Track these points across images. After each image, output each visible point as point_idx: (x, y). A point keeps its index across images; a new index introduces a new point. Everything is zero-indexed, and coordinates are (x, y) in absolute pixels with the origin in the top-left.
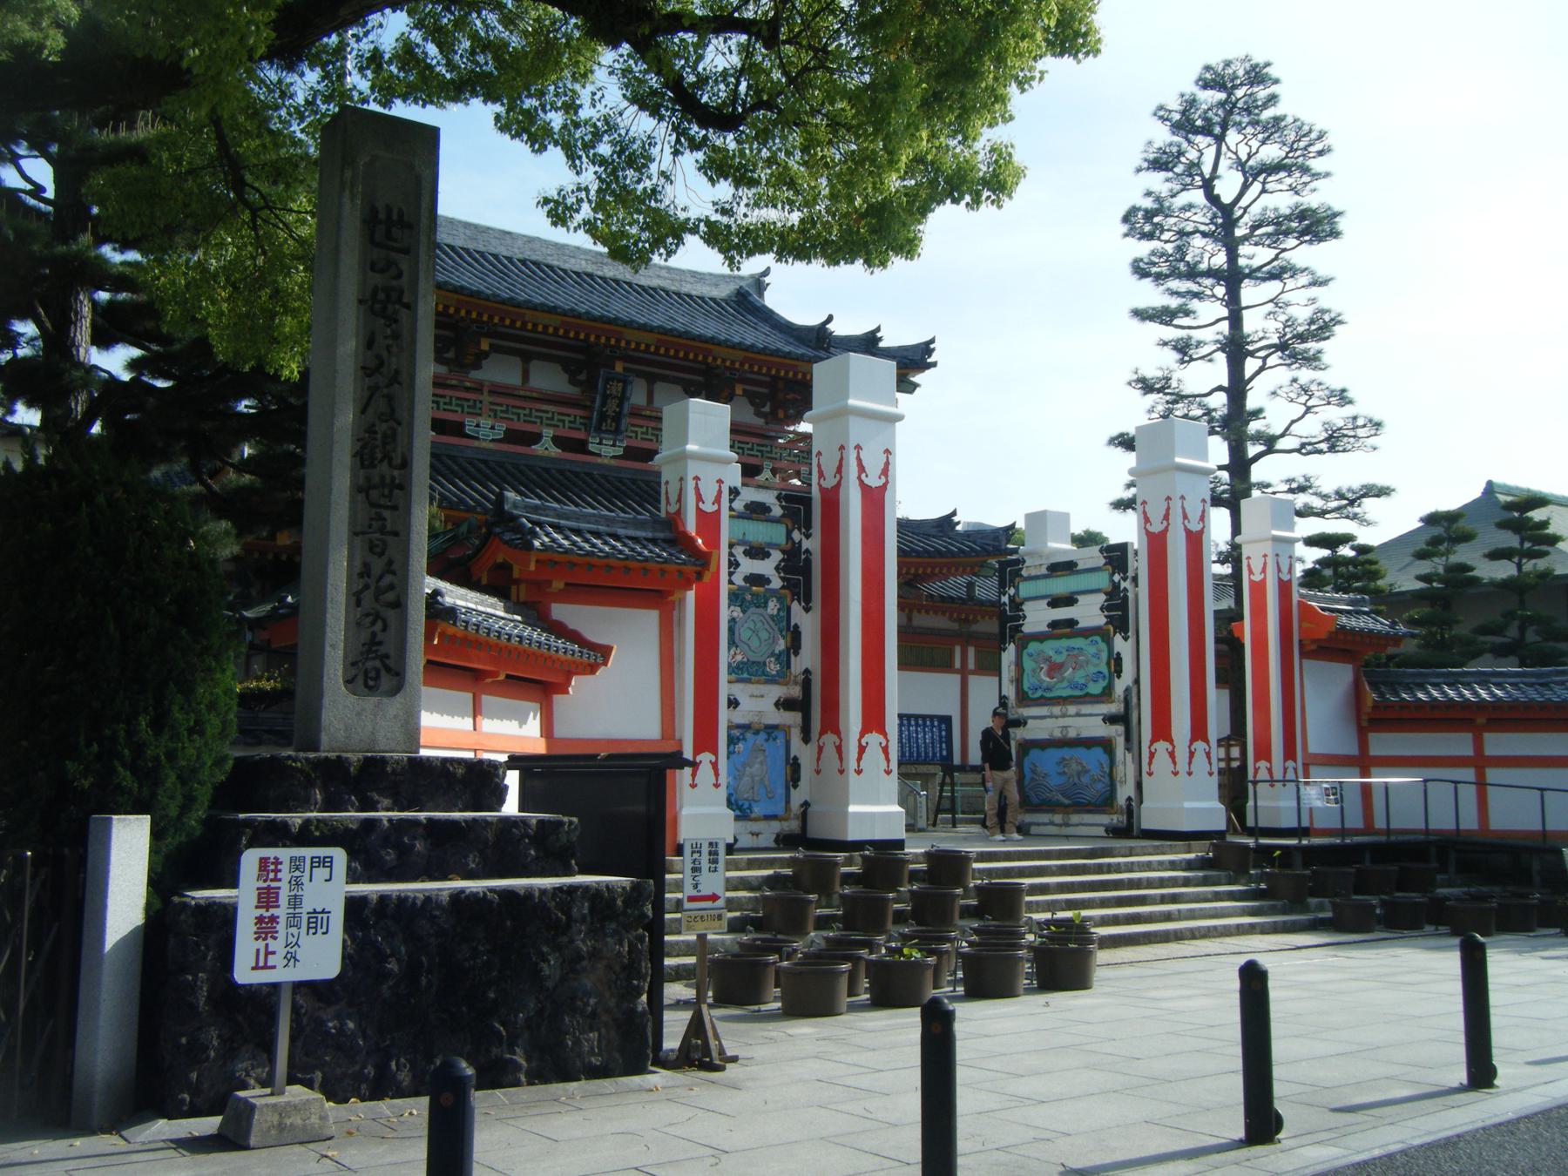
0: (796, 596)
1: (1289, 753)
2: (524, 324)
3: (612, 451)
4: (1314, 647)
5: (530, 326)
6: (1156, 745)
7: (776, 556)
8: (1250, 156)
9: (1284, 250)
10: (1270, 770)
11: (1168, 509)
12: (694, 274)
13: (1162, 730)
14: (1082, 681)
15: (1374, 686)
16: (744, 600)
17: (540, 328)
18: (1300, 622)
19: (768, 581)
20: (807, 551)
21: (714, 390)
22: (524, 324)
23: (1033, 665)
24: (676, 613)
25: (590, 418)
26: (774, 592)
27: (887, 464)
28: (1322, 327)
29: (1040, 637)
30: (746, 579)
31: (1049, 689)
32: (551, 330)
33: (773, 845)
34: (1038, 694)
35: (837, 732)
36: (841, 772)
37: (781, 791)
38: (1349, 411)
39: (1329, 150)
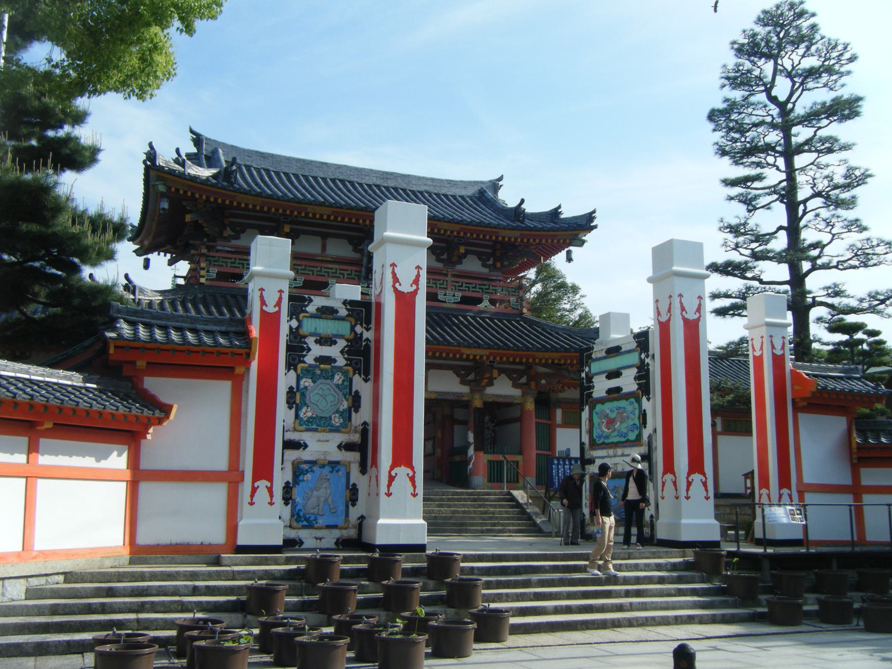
0: (357, 370)
1: (784, 481)
2: (307, 214)
4: (805, 404)
5: (311, 215)
7: (342, 343)
8: (793, 68)
9: (820, 128)
11: (670, 304)
12: (449, 182)
14: (625, 431)
15: (862, 432)
17: (318, 216)
18: (793, 385)
19: (335, 361)
20: (367, 339)
21: (272, 227)
22: (307, 214)
24: (244, 382)
25: (361, 272)
26: (339, 369)
27: (700, 305)
28: (855, 179)
29: (602, 401)
30: (316, 360)
31: (607, 437)
32: (325, 217)
33: (334, 546)
34: (602, 440)
35: (673, 473)
37: (342, 508)
38: (865, 235)
39: (856, 58)
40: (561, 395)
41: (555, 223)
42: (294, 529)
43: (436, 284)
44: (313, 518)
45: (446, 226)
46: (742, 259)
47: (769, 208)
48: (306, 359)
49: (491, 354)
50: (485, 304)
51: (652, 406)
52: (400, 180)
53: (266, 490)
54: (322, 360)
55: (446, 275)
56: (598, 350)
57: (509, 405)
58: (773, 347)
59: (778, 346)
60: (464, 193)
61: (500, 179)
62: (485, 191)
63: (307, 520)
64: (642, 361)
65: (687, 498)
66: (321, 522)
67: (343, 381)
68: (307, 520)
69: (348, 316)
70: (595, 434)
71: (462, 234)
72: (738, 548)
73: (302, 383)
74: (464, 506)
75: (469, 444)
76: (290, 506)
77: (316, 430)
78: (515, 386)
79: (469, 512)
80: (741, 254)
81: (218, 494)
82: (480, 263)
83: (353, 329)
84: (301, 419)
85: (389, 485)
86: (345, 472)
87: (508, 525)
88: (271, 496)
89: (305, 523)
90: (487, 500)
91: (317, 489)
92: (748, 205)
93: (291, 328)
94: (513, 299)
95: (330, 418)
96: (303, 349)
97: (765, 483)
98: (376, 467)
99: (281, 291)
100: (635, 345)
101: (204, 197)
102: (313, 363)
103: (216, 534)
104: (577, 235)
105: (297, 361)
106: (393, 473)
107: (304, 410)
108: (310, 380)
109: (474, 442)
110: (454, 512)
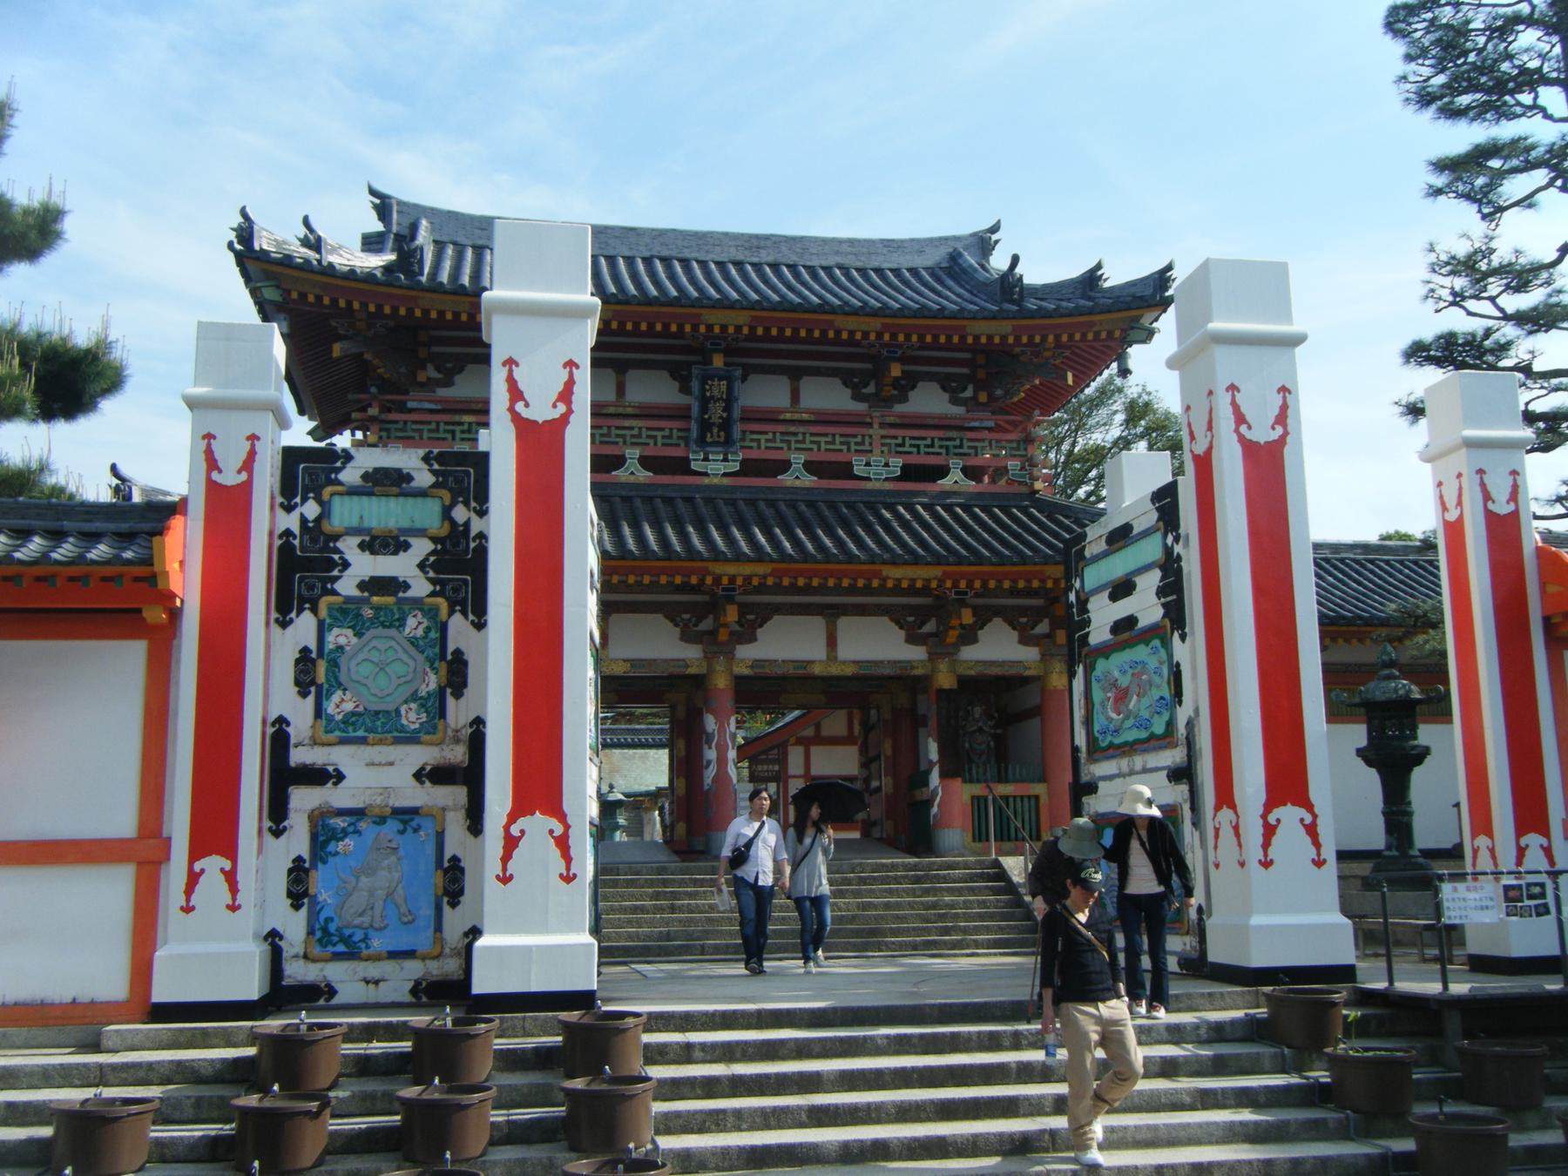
3: (722, 468)
7: (421, 548)
10: (1548, 851)
16: (359, 615)
25: (688, 430)
26: (417, 603)
27: (1284, 408)
29: (1105, 650)
30: (362, 586)
33: (408, 998)
35: (1233, 806)
37: (427, 912)
41: (1090, 299)
42: (314, 961)
43: (848, 444)
44: (358, 936)
45: (850, 323)
46: (1477, 325)
47: (1530, 206)
48: (338, 586)
49: (947, 575)
50: (954, 479)
51: (1189, 652)
53: (222, 877)
54: (376, 585)
55: (870, 425)
56: (1096, 535)
57: (1025, 681)
58: (1487, 497)
60: (920, 262)
61: (995, 229)
62: (960, 255)
63: (346, 940)
64: (1168, 551)
65: (1267, 864)
66: (378, 944)
67: (428, 630)
69: (435, 485)
70: (1096, 727)
71: (887, 337)
72: (1391, 981)
74: (891, 892)
75: (931, 764)
76: (304, 910)
77: (363, 741)
78: (1025, 640)
79: (898, 906)
80: (1470, 313)
81: (112, 889)
82: (848, 392)
83: (446, 513)
84: (330, 719)
85: (506, 858)
86: (432, 832)
87: (977, 930)
89: (341, 948)
90: (945, 879)
91: (370, 871)
92: (1479, 202)
94: (1013, 464)
95: (398, 712)
96: (331, 564)
97: (1482, 824)
100: (1155, 515)
102: (356, 593)
103: (112, 984)
104: (1137, 319)
105: (317, 591)
106: (515, 831)
107: (336, 697)
108: (350, 632)
109: (940, 761)
110: (865, 907)
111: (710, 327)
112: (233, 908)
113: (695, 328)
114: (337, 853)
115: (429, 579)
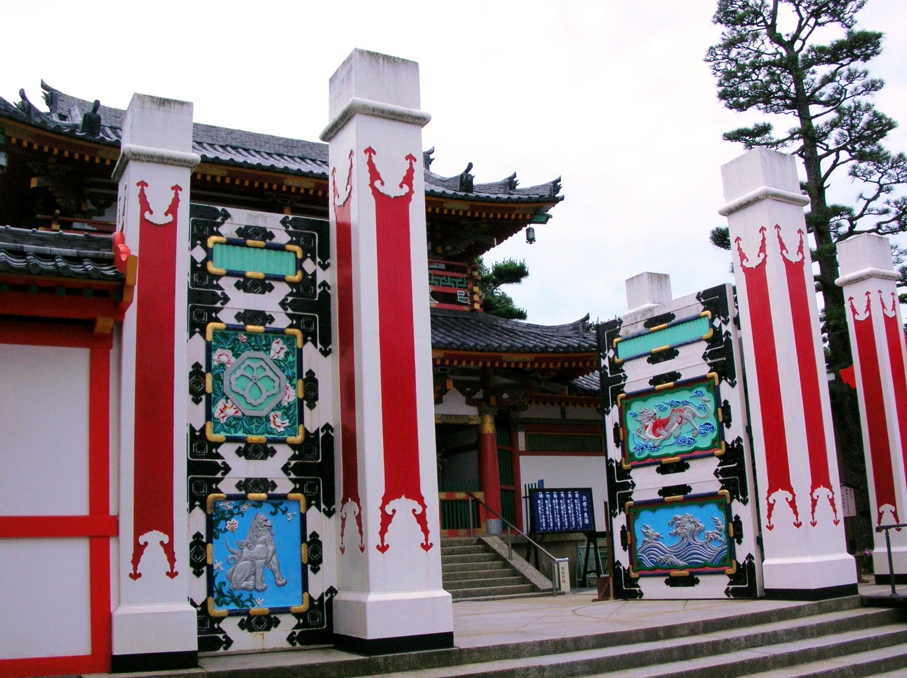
6: (774, 496)
7: (281, 291)
13: (780, 479)
19: (271, 319)
20: (324, 284)
23: (639, 426)
24: (113, 353)
26: (280, 332)
29: (642, 395)
30: (238, 317)
36: (362, 549)
40: (523, 415)
51: (741, 396)
52: (308, 149)
53: (162, 549)
59: (889, 306)
67: (287, 354)
68: (236, 601)
73: (215, 356)
78: (470, 402)
83: (299, 264)
84: (217, 422)
88: (172, 560)
89: (233, 606)
93: (193, 262)
95: (267, 418)
98: (356, 499)
99: (177, 188)
101: (56, 151)
107: (220, 404)
108: (230, 353)
111: (289, 188)
112: (172, 574)
113: (280, 187)
114: (226, 530)
115: (287, 314)
